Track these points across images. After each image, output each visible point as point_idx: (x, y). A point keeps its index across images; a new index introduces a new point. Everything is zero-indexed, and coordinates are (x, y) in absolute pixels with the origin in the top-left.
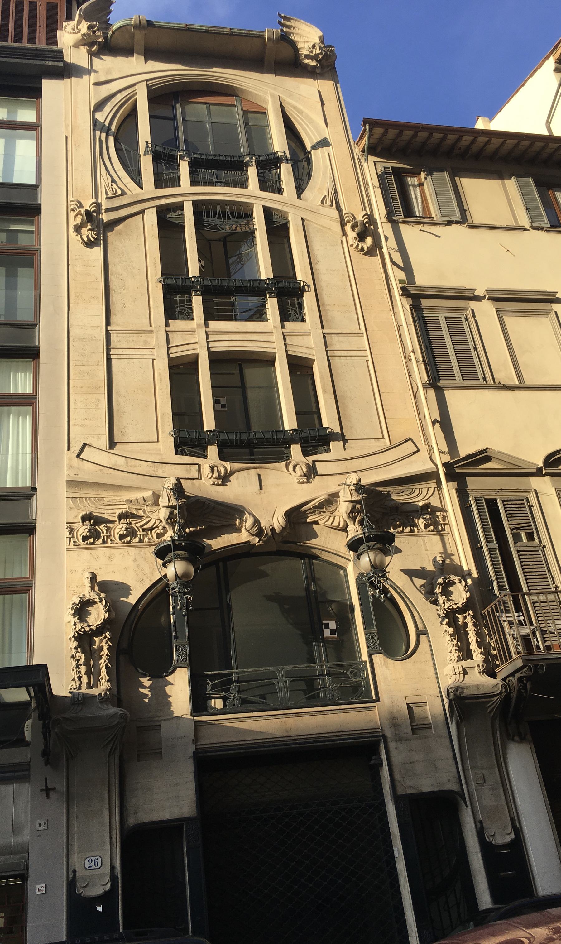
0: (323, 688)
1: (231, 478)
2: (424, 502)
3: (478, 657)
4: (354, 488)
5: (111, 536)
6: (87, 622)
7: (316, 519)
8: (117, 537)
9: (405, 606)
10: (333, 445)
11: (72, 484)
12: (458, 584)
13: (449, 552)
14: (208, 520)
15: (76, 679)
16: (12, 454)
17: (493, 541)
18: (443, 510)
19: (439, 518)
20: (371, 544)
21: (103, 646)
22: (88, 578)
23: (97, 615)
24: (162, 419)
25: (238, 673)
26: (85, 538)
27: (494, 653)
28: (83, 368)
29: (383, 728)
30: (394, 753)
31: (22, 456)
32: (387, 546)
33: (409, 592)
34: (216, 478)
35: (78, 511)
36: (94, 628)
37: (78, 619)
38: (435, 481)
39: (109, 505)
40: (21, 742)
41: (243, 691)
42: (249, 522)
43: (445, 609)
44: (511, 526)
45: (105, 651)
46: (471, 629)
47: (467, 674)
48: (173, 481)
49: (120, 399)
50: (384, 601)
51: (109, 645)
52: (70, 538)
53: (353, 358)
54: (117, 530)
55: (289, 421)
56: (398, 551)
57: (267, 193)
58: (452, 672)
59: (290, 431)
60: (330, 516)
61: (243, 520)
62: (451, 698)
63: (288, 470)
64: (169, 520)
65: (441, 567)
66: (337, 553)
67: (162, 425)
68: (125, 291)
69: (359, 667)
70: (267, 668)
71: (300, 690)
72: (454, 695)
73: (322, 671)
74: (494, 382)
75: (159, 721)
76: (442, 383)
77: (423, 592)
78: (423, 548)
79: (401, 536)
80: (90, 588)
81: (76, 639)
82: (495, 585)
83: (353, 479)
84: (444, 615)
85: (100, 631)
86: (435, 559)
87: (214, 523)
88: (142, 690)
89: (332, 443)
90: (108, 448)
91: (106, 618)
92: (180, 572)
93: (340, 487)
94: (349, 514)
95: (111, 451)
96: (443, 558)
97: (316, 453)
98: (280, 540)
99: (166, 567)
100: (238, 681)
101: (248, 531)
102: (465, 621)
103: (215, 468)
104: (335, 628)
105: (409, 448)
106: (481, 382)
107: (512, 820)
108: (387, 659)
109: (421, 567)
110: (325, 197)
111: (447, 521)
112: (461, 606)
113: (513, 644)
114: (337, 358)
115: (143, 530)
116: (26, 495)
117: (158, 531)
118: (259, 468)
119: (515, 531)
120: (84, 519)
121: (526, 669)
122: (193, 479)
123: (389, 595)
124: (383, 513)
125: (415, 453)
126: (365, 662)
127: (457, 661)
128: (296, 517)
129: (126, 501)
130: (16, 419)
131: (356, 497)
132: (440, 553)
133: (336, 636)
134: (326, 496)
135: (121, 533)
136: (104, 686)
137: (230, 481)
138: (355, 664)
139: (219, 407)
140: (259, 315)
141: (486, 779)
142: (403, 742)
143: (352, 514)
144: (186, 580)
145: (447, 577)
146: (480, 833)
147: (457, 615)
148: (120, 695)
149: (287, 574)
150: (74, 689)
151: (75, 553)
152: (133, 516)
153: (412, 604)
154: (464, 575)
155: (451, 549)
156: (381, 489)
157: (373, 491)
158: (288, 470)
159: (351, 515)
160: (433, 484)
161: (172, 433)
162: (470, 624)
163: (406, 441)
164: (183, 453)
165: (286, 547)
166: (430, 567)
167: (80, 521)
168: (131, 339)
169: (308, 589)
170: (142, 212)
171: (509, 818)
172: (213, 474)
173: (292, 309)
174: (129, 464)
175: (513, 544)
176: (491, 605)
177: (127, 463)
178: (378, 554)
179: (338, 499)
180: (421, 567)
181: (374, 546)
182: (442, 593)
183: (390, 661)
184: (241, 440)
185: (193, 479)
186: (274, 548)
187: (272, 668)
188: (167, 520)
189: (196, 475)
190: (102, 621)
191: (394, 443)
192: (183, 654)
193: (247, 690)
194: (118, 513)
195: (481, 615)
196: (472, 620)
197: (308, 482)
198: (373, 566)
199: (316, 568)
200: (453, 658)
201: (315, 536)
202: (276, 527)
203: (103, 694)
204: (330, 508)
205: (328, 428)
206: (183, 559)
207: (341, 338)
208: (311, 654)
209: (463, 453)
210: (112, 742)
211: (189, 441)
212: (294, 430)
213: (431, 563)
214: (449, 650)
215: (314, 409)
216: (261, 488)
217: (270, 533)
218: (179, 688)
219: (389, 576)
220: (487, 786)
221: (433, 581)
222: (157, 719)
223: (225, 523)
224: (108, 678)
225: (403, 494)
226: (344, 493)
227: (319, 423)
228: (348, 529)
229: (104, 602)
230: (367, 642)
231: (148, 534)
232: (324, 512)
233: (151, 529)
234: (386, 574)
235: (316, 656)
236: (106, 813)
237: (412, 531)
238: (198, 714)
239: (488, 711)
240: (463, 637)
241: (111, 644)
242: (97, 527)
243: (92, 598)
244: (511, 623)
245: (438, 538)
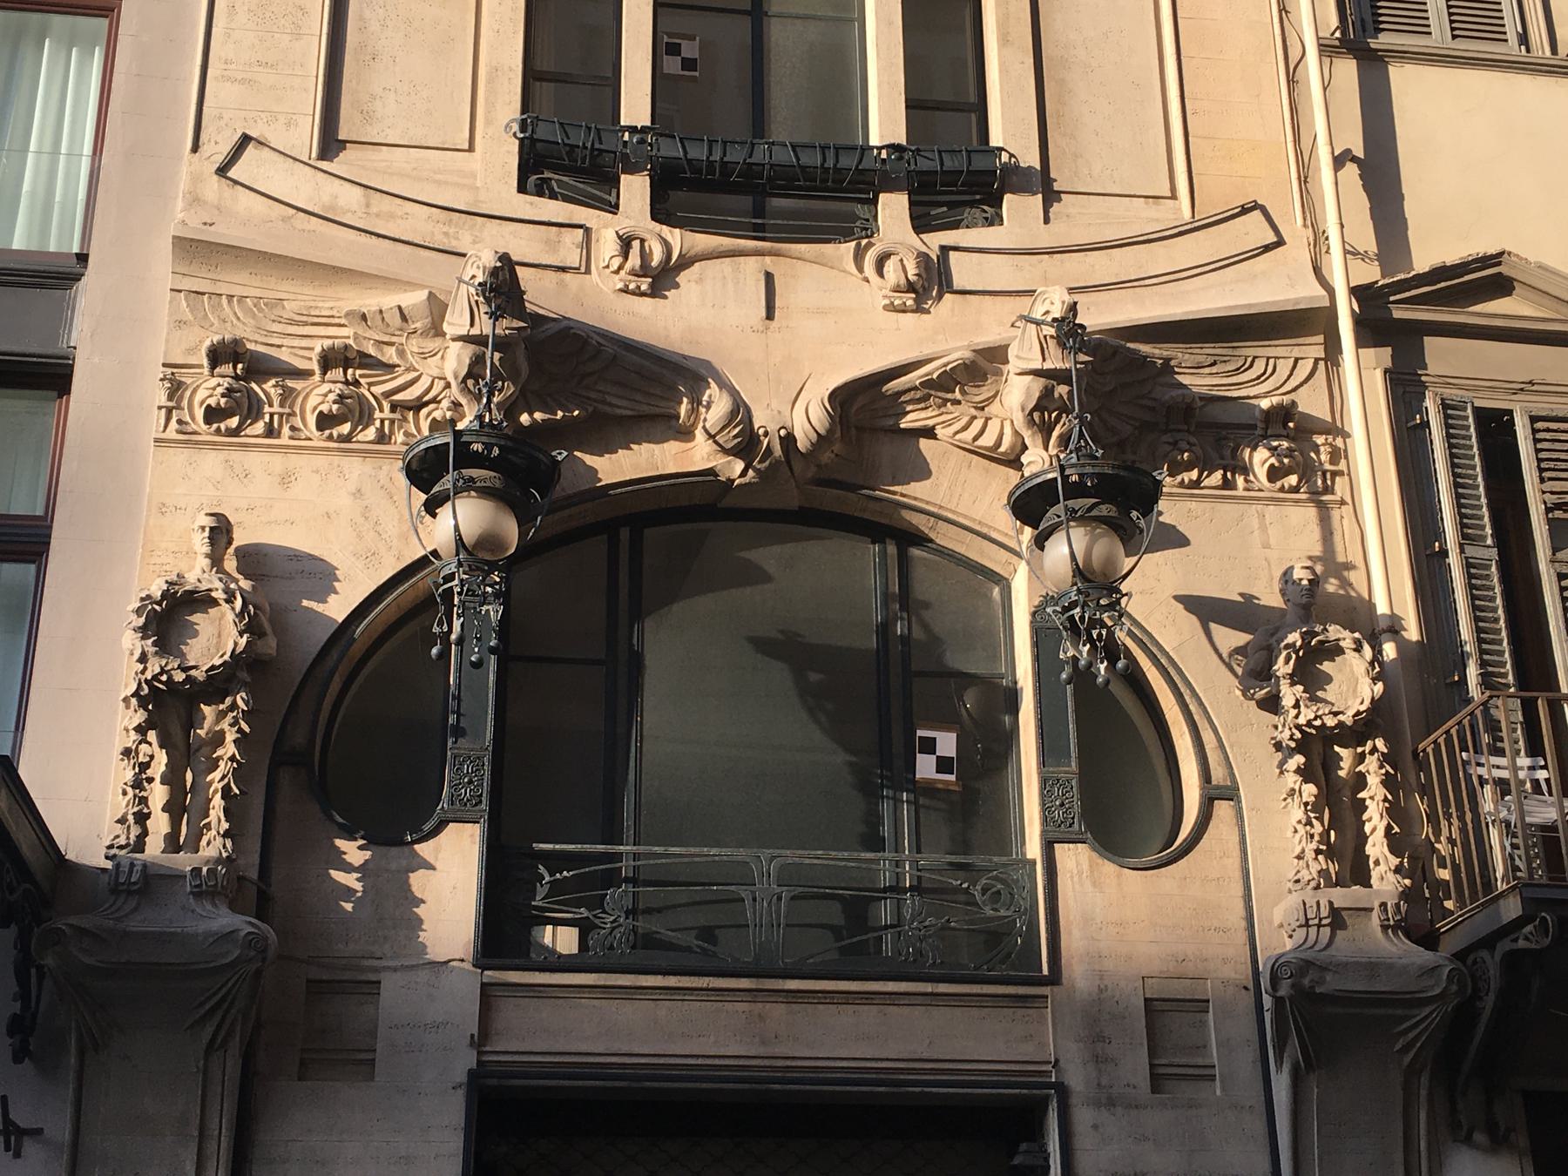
0: (892, 926)
1: (682, 278)
2: (1275, 400)
3: (1386, 878)
4: (1052, 331)
5: (293, 414)
6: (182, 655)
7: (930, 423)
8: (312, 420)
9: (1176, 708)
10: (1010, 203)
11: (191, 249)
12: (1350, 655)
13: (1341, 559)
14: (593, 395)
15: (131, 818)
16: (38, 152)
17: (1484, 538)
18: (1335, 429)
19: (1318, 453)
20: (1079, 503)
21: (222, 732)
22: (203, 528)
23: (215, 639)
24: (490, 81)
25: (636, 856)
26: (212, 415)
27: (1445, 874)
29: (1062, 1063)
30: (1084, 1140)
31: (68, 162)
32: (1134, 514)
33: (1197, 671)
34: (633, 273)
35: (202, 333)
36: (199, 675)
37: (155, 644)
38: (1320, 338)
39: (298, 323)
41: (648, 911)
42: (717, 408)
43: (1298, 727)
44: (1547, 497)
45: (229, 749)
46: (1374, 794)
47: (1343, 926)
48: (490, 260)
49: (367, 14)
50: (1107, 682)
51: (240, 731)
52: (169, 411)
54: (313, 401)
55: (884, 121)
56: (1173, 539)
58: (1296, 917)
59: (880, 148)
60: (974, 418)
61: (699, 403)
62: (1281, 993)
63: (860, 269)
64: (470, 382)
65: (1304, 600)
66: (985, 530)
67: (486, 100)
69: (1009, 882)
70: (724, 851)
71: (823, 926)
72: (1293, 986)
73: (899, 877)
74: (1554, 50)
75: (376, 970)
76: (1384, 40)
77: (1239, 671)
79: (1192, 496)
80: (208, 561)
81: (143, 702)
82: (1472, 672)
83: (1053, 303)
84: (1293, 745)
85: (217, 685)
86: (1288, 573)
87: (610, 405)
88: (337, 875)
89: (1007, 197)
90: (314, 155)
91: (240, 649)
92: (470, 533)
93: (1014, 332)
94: (1031, 414)
95: (324, 165)
96: (1314, 572)
97: (955, 226)
98: (810, 475)
99: (434, 515)
100: (633, 881)
101: (711, 436)
102: (1361, 768)
103: (636, 244)
104: (953, 754)
105: (1253, 230)
106: (1513, 48)
108: (1100, 861)
109: (1241, 595)
111: (1342, 466)
112: (1349, 722)
113: (1503, 848)
115: (393, 409)
116: (57, 277)
117: (437, 415)
118: (771, 253)
119: (1558, 514)
120: (217, 356)
121: (1529, 928)
122: (563, 269)
123: (1120, 665)
124: (1138, 423)
125: (1267, 248)
126: (1034, 862)
127: (1317, 887)
128: (866, 408)
129: (347, 315)
130: (63, 54)
131: (1056, 361)
132: (1310, 558)
133: (952, 778)
134: (967, 354)
135: (325, 408)
136: (213, 846)
137: (677, 286)
138: (997, 867)
139: (672, 65)
142: (1119, 1110)
143: (1043, 413)
144: (488, 557)
145: (1318, 628)
147: (1337, 748)
148: (266, 878)
149: (830, 582)
150: (121, 847)
151: (180, 456)
152: (365, 361)
153: (1201, 704)
154: (1374, 630)
155: (1347, 550)
156: (1145, 349)
157: (1116, 351)
158: (860, 269)
159: (1036, 415)
160: (1313, 348)
161: (516, 127)
162: (1374, 781)
163: (1244, 211)
165: (830, 499)
166: (1271, 598)
167: (205, 362)
169: (884, 629)
172: (626, 258)
174: (374, 210)
175: (1549, 552)
176: (1445, 728)
177: (368, 205)
178: (1101, 536)
179: (1005, 368)
180: (1241, 595)
181: (1090, 509)
182: (1294, 679)
183: (1109, 868)
184: (724, 164)
185: (563, 269)
186: (793, 501)
187: (741, 854)
188: (464, 381)
189: (573, 259)
190: (227, 657)
191: (1206, 211)
192: (470, 782)
193: (659, 911)
194: (318, 349)
195: (1415, 754)
196: (1381, 767)
197: (919, 309)
198: (1080, 573)
199: (919, 574)
200: (1305, 875)
201: (921, 471)
202: (798, 434)
203: (205, 869)
204: (975, 390)
205: (1001, 149)
206: (486, 492)
208: (874, 821)
209: (1423, 261)
210: (219, 1014)
211: (563, 155)
212: (893, 147)
213: (1277, 587)
214: (1298, 850)
215: (973, 99)
216: (770, 315)
217: (778, 450)
218: (449, 877)
219: (1132, 606)
221: (1273, 641)
222: (375, 963)
223: (646, 409)
224: (225, 825)
225: (1214, 369)
226: (1021, 347)
227: (979, 130)
228: (1024, 459)
229: (239, 603)
230: (1043, 804)
231: (405, 419)
232: (957, 402)
233: (417, 406)
234: (1118, 602)
235: (886, 830)
237: (1227, 484)
238: (497, 961)
239: (1397, 1047)
240: (1349, 816)
241: (247, 729)
242: (254, 385)
243: (204, 586)
244: (1503, 787)
245: (1311, 512)
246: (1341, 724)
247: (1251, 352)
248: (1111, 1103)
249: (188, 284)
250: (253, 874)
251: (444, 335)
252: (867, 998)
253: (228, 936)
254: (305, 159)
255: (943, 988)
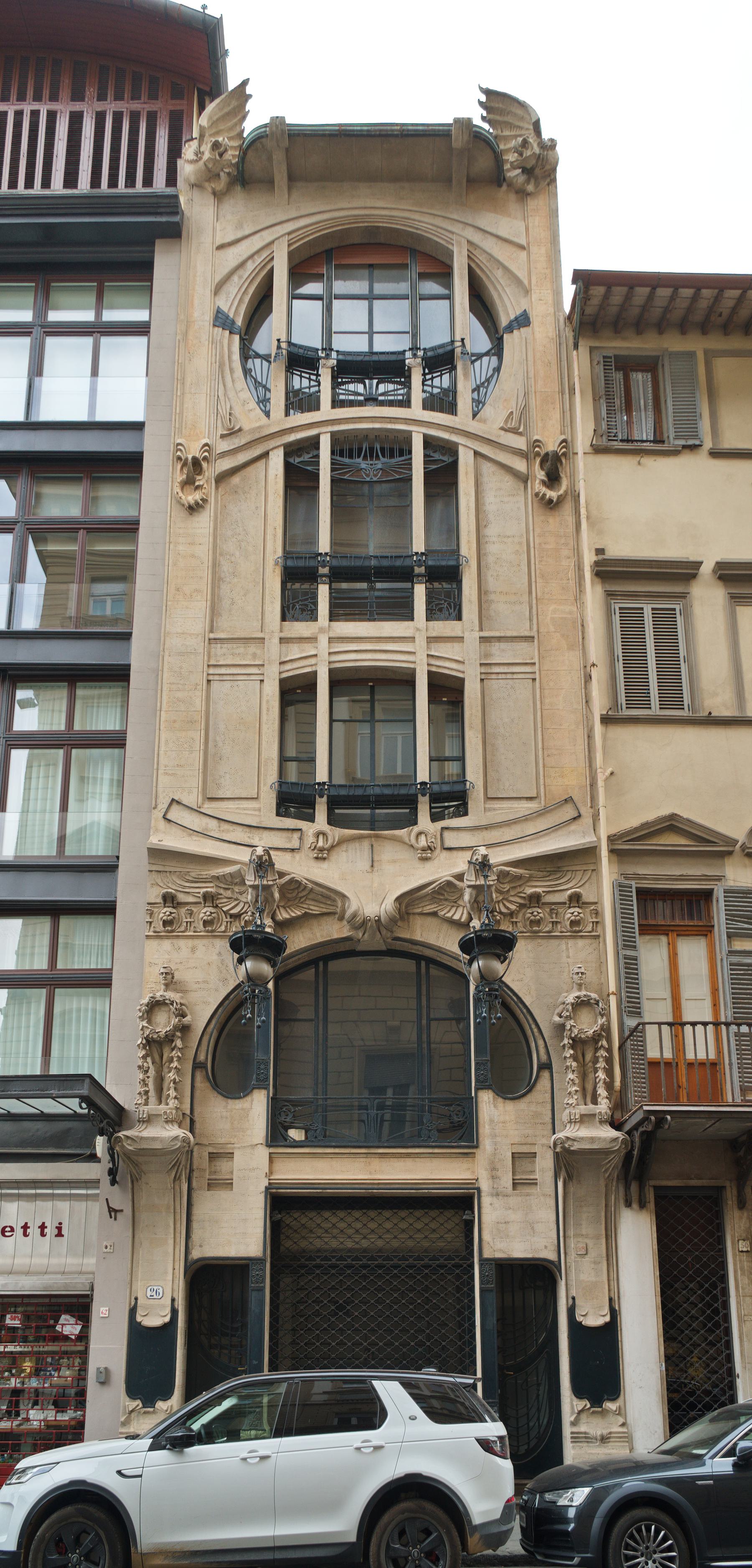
7: (435, 910)
14: (305, 906)
28: (180, 695)
40: (93, 1158)
53: (515, 676)
57: (432, 413)
68: (236, 580)
75: (234, 1148)
78: (564, 954)
105: (568, 812)
107: (611, 1300)
110: (512, 413)
114: (494, 676)
117: (247, 918)
125: (575, 819)
140: (404, 611)
141: (589, 1249)
142: (500, 1197)
146: (571, 1311)
164: (287, 815)
168: (237, 651)
170: (265, 455)
171: (607, 1298)
173: (445, 601)
183: (500, 1100)
207: (503, 645)
220: (587, 1259)
236: (171, 1242)
246: (587, 1037)
247: (574, 868)
248: (497, 1195)
249: (154, 868)
250: (188, 1112)
251: (245, 884)
252: (408, 1155)
253: (176, 1138)
254: (195, 808)
255: (436, 1151)
